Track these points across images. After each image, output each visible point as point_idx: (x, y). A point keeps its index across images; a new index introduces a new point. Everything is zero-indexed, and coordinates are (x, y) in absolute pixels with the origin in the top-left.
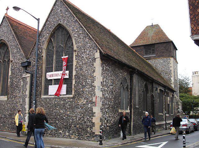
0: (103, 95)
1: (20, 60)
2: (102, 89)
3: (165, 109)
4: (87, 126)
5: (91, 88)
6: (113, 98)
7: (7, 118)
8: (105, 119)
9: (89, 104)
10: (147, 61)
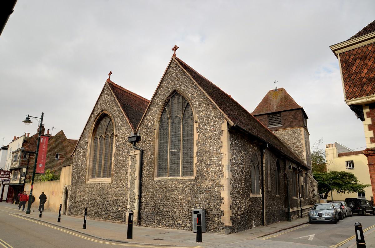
0: (233, 176)
1: (127, 134)
2: (231, 168)
3: (299, 192)
4: (214, 215)
5: (217, 168)
6: (244, 180)
7: (111, 205)
8: (236, 207)
9: (216, 188)
10: (273, 132)
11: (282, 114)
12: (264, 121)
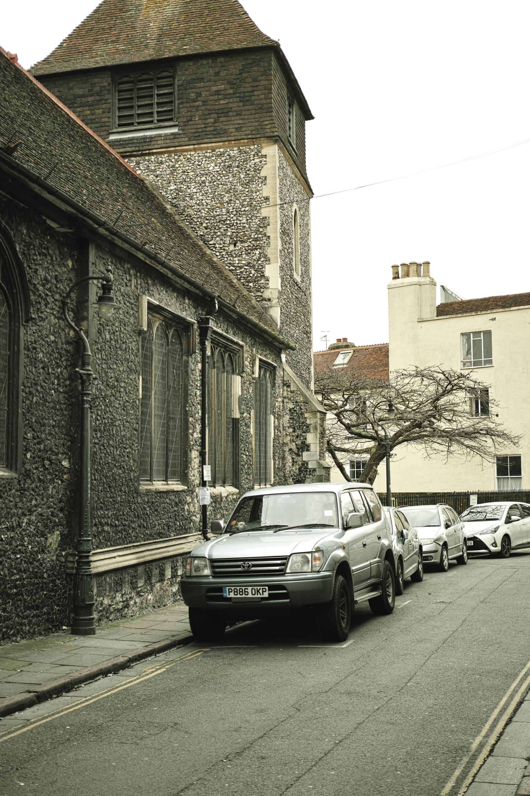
3: (202, 454)
10: (131, 164)
11: (179, 73)
12: (90, 105)
